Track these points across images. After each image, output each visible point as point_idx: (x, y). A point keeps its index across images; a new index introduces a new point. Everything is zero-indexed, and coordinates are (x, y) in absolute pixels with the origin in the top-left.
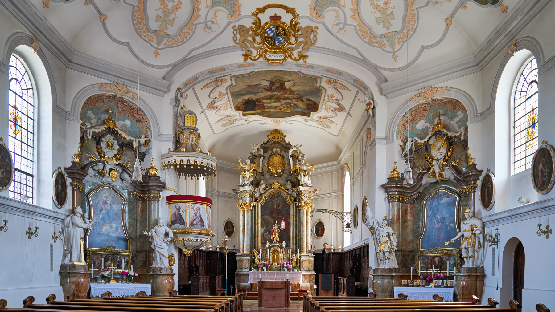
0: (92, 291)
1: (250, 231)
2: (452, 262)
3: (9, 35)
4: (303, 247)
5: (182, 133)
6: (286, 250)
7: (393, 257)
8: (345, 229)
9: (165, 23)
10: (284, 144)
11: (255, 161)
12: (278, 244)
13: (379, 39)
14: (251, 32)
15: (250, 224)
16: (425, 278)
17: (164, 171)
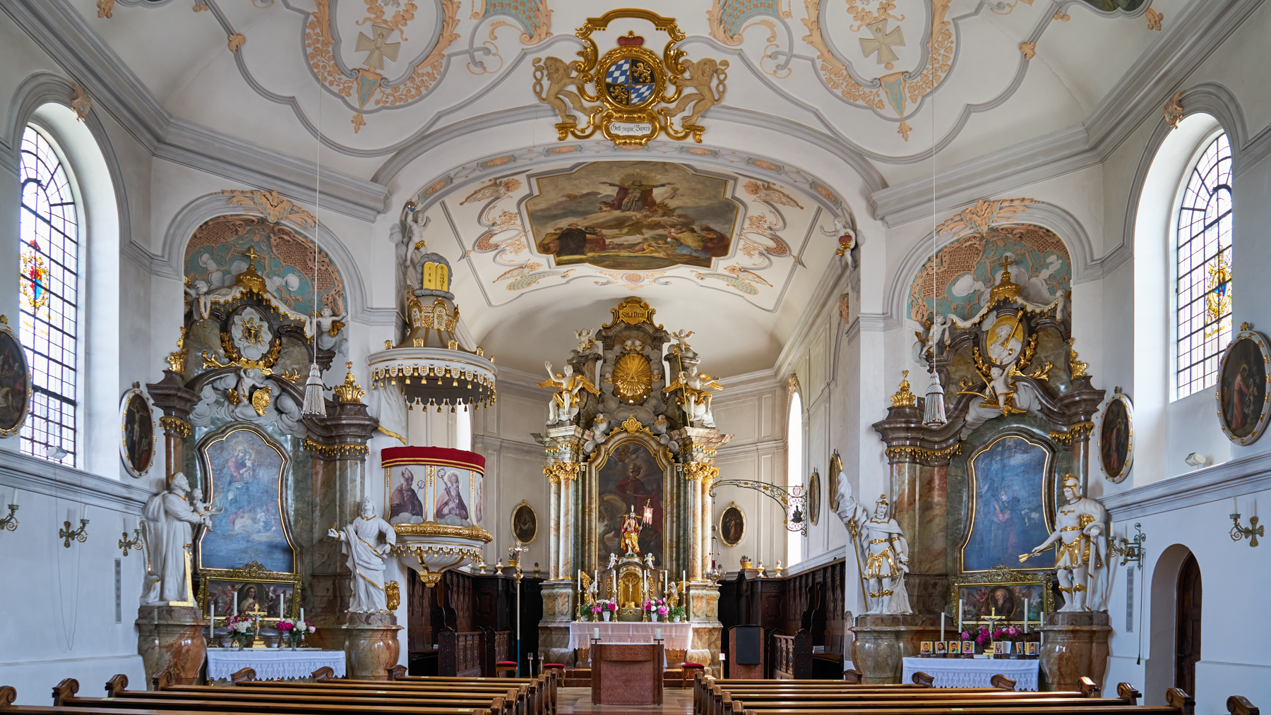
0: (212, 666)
1: (571, 529)
2: (1035, 600)
3: (21, 80)
4: (693, 567)
5: (417, 304)
6: (655, 572)
7: (900, 589)
8: (791, 524)
9: (377, 52)
10: (651, 331)
11: (585, 369)
12: (637, 560)
13: (867, 90)
14: (574, 74)
15: (572, 513)
16: (973, 637)
17: (376, 393)
